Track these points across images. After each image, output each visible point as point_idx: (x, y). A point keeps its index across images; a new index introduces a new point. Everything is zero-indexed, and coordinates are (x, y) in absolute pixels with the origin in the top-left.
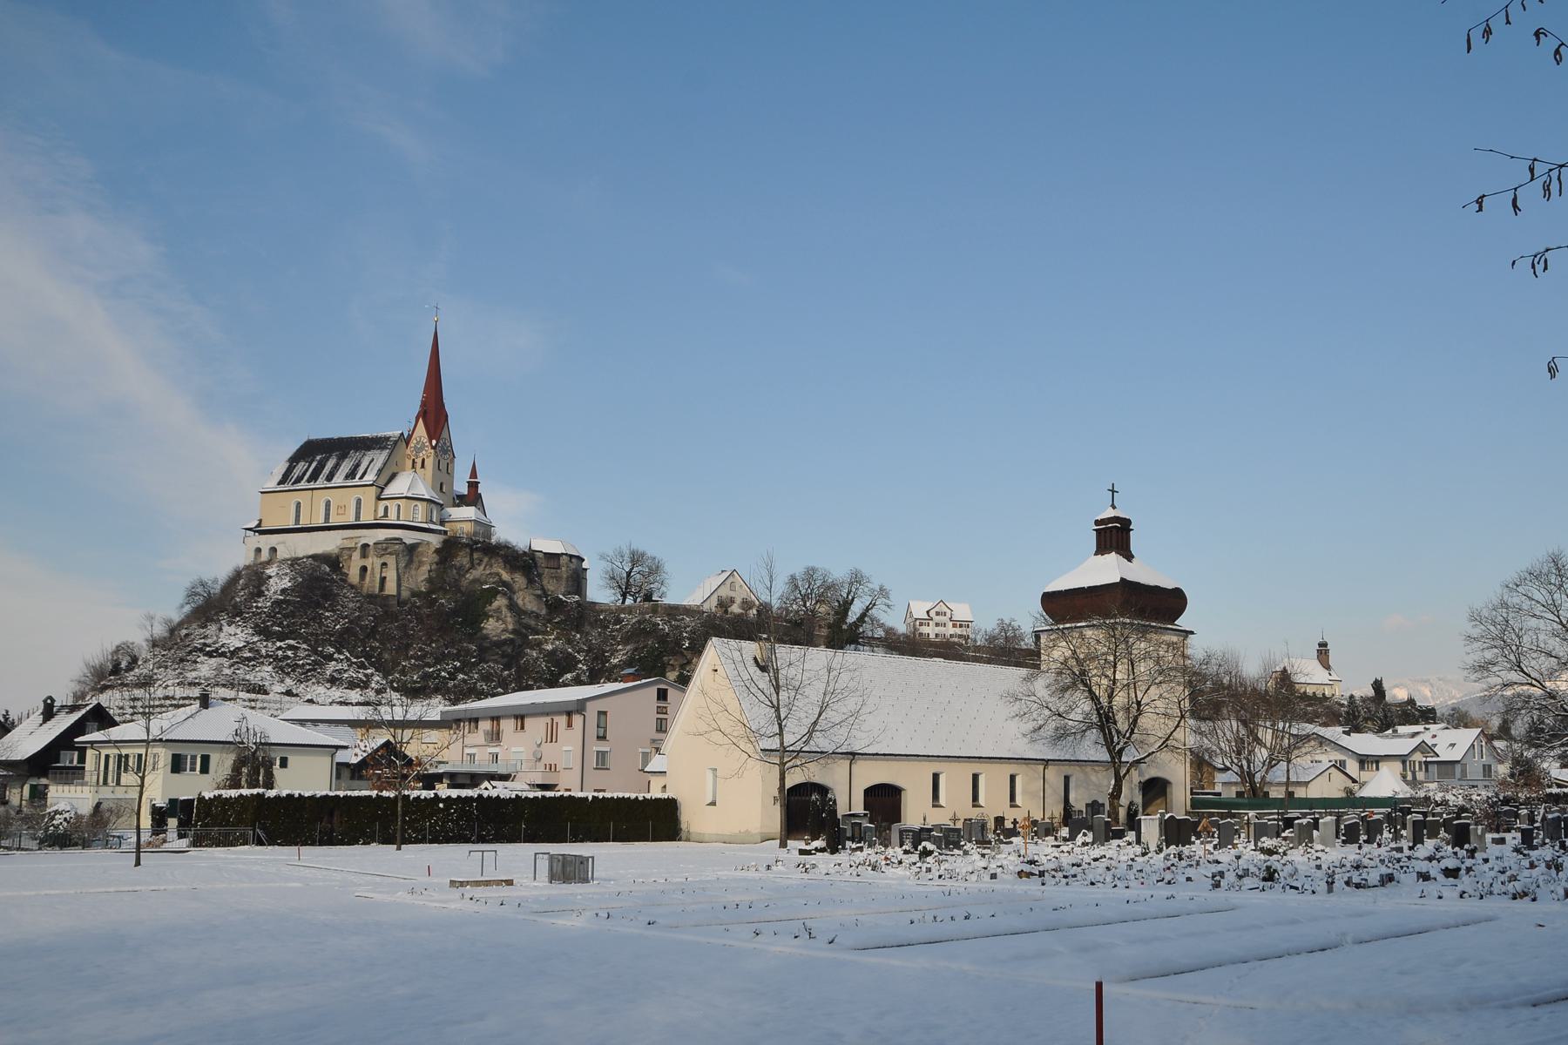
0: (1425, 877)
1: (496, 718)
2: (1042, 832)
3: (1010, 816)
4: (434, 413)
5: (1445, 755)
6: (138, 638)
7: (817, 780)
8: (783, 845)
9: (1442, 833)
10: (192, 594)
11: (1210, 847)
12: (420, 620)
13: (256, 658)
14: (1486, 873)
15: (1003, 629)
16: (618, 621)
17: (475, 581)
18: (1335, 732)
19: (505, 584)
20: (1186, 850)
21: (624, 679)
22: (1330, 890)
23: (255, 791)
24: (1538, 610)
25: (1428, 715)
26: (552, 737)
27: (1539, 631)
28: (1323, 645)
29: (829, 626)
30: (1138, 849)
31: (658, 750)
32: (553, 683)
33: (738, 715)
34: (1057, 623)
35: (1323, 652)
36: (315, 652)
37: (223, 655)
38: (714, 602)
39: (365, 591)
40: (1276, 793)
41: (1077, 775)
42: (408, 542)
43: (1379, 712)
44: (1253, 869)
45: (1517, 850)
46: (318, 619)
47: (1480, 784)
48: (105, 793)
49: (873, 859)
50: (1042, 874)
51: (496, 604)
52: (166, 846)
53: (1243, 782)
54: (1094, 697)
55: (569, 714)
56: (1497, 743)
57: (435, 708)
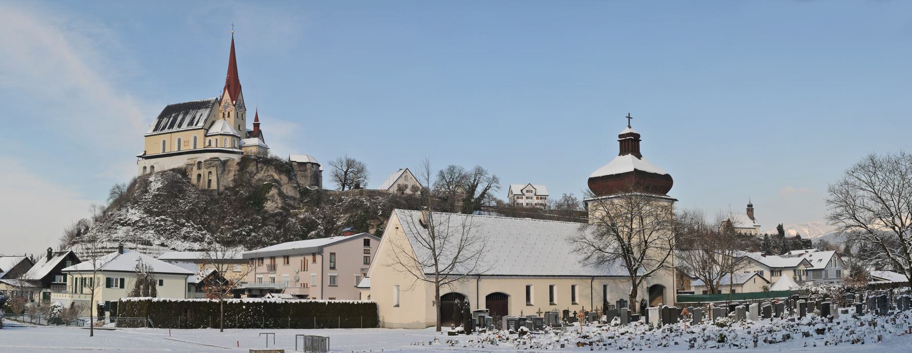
0: (806, 335)
1: (273, 258)
2: (591, 318)
3: (572, 309)
4: (233, 86)
5: (817, 266)
6: (89, 217)
7: (458, 291)
8: (439, 329)
9: (816, 310)
10: (113, 193)
11: (688, 324)
12: (230, 203)
13: (145, 227)
14: (838, 330)
15: (566, 200)
16: (341, 200)
17: (259, 180)
18: (757, 255)
19: (276, 181)
20: (674, 326)
21: (344, 234)
22: (756, 346)
23: (147, 298)
24: (864, 186)
25: (807, 244)
26: (304, 268)
27: (864, 197)
28: (750, 206)
29: (464, 200)
30: (647, 327)
31: (365, 275)
32: (304, 237)
33: (410, 254)
34: (598, 195)
35: (750, 209)
36: (176, 222)
37: (129, 225)
38: (395, 188)
39: (200, 188)
40: (725, 291)
41: (610, 284)
42: (222, 159)
43: (781, 243)
44: (712, 336)
45: (854, 317)
46: (176, 204)
47: (835, 281)
48: (76, 297)
49: (492, 337)
50: (591, 344)
51: (271, 193)
52: (105, 326)
53: (707, 285)
54: (620, 239)
55: (314, 255)
56: (844, 259)
57: (239, 252)
